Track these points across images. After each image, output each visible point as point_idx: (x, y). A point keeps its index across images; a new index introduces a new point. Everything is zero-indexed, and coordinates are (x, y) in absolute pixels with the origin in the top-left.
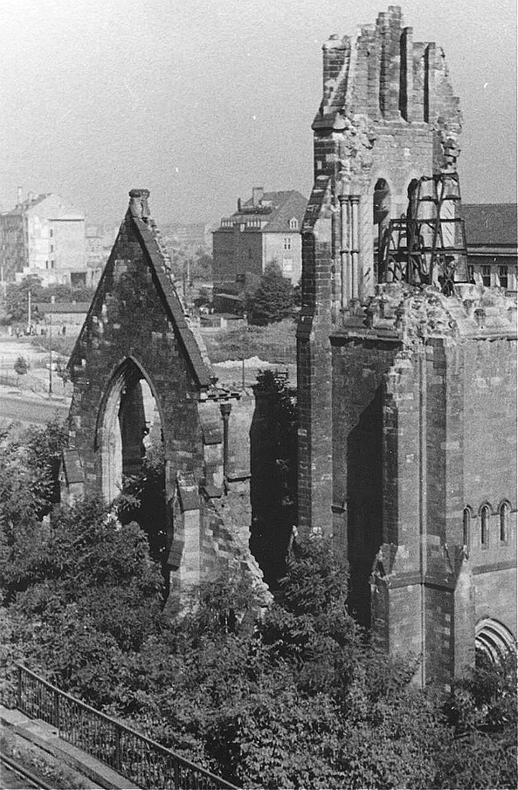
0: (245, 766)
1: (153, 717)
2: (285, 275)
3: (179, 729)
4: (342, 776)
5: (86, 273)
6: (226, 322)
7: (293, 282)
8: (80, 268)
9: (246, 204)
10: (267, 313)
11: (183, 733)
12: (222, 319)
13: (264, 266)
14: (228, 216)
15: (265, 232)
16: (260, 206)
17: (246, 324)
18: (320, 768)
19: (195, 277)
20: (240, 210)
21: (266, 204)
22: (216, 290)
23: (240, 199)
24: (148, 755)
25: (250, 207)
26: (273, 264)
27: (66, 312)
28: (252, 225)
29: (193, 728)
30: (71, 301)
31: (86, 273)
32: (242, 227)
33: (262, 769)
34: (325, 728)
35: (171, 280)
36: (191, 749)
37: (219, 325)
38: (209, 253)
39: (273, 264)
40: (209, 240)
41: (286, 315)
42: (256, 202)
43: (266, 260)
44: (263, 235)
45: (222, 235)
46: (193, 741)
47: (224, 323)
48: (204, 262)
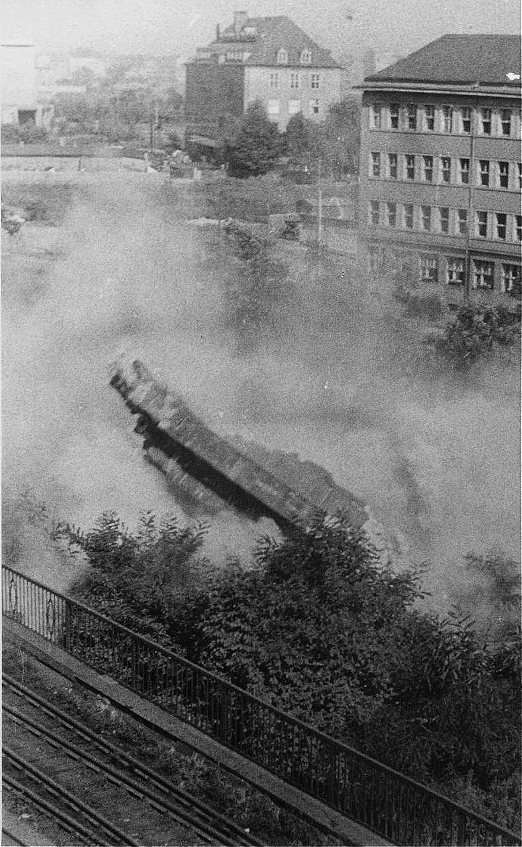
0: (209, 650)
1: (109, 598)
2: (272, 119)
3: (138, 612)
4: (350, 671)
5: (35, 111)
6: (200, 172)
7: (279, 128)
8: (28, 105)
9: (227, 31)
10: (249, 163)
11: (143, 615)
12: (195, 169)
13: (246, 107)
14: (205, 44)
15: (249, 66)
16: (243, 34)
17: (224, 177)
18: (294, 657)
19: (166, 119)
20: (219, 38)
21: (250, 31)
22: (188, 134)
23: (218, 25)
24: (102, 638)
25: (232, 34)
26: (257, 106)
27: (11, 156)
28: (232, 57)
29: (155, 611)
30: (18, 142)
31: (35, 111)
32: (222, 60)
33: (229, 656)
34: (301, 615)
35: (172, 478)
36: (152, 635)
37: (192, 176)
38: (181, 91)
39: (257, 106)
40: (181, 77)
41: (271, 167)
42: (238, 27)
43: (249, 100)
44: (246, 70)
45: (195, 69)
46: (155, 626)
47: (198, 174)
48: (176, 101)
